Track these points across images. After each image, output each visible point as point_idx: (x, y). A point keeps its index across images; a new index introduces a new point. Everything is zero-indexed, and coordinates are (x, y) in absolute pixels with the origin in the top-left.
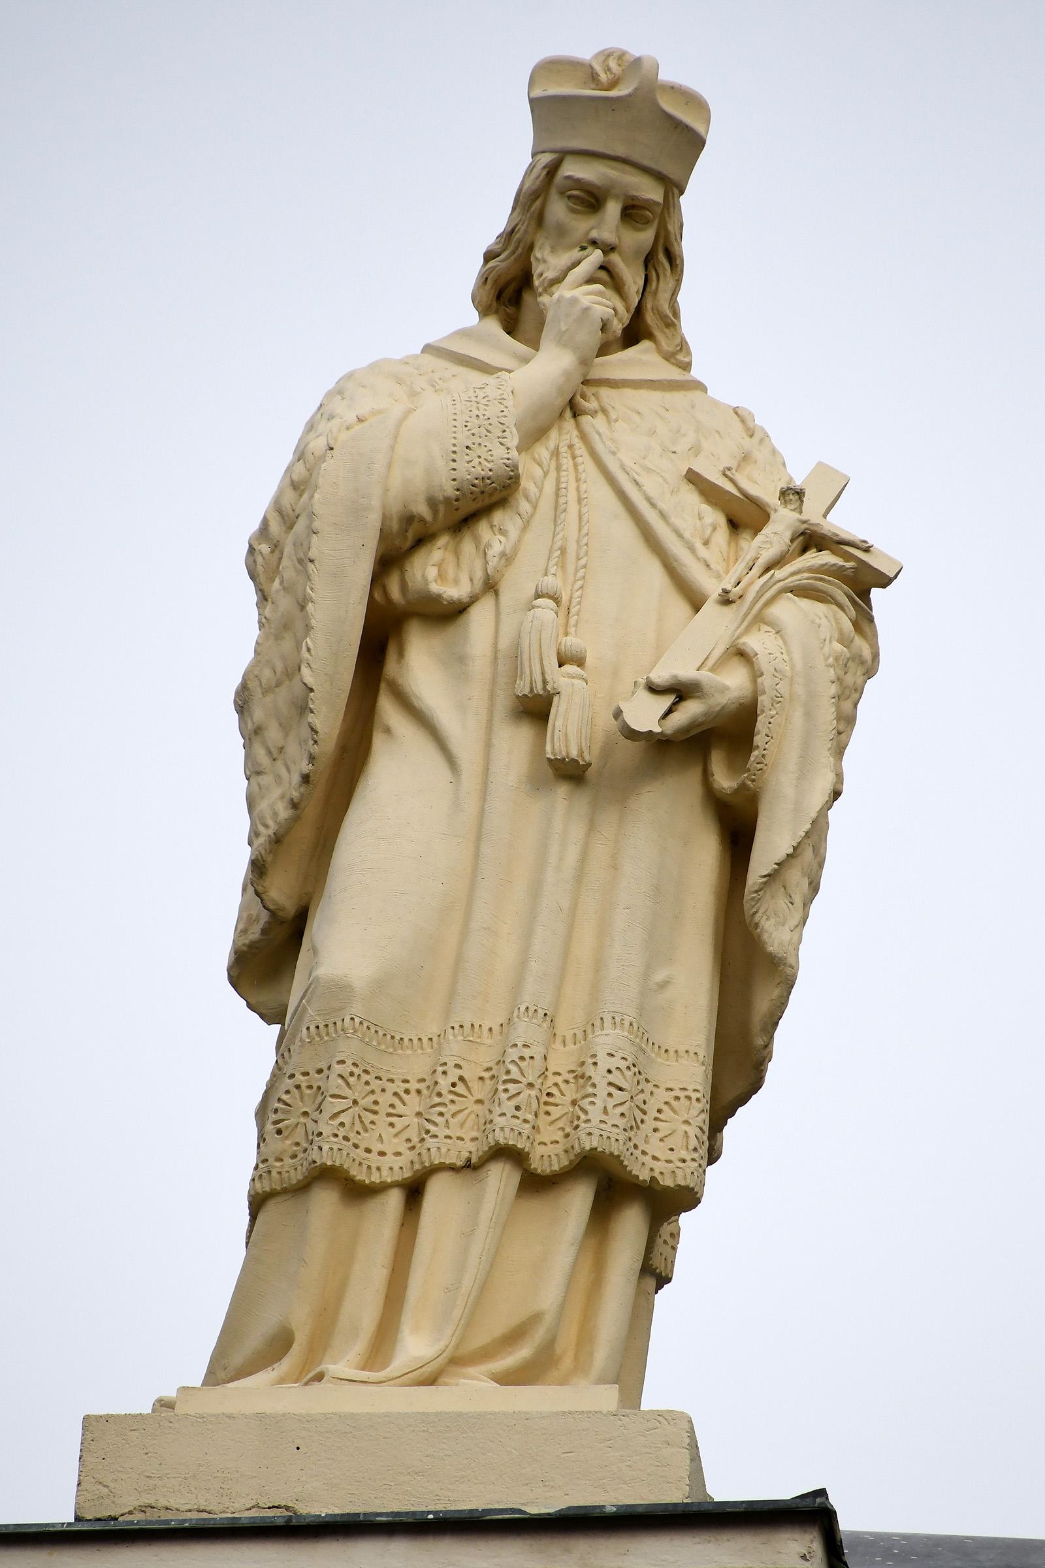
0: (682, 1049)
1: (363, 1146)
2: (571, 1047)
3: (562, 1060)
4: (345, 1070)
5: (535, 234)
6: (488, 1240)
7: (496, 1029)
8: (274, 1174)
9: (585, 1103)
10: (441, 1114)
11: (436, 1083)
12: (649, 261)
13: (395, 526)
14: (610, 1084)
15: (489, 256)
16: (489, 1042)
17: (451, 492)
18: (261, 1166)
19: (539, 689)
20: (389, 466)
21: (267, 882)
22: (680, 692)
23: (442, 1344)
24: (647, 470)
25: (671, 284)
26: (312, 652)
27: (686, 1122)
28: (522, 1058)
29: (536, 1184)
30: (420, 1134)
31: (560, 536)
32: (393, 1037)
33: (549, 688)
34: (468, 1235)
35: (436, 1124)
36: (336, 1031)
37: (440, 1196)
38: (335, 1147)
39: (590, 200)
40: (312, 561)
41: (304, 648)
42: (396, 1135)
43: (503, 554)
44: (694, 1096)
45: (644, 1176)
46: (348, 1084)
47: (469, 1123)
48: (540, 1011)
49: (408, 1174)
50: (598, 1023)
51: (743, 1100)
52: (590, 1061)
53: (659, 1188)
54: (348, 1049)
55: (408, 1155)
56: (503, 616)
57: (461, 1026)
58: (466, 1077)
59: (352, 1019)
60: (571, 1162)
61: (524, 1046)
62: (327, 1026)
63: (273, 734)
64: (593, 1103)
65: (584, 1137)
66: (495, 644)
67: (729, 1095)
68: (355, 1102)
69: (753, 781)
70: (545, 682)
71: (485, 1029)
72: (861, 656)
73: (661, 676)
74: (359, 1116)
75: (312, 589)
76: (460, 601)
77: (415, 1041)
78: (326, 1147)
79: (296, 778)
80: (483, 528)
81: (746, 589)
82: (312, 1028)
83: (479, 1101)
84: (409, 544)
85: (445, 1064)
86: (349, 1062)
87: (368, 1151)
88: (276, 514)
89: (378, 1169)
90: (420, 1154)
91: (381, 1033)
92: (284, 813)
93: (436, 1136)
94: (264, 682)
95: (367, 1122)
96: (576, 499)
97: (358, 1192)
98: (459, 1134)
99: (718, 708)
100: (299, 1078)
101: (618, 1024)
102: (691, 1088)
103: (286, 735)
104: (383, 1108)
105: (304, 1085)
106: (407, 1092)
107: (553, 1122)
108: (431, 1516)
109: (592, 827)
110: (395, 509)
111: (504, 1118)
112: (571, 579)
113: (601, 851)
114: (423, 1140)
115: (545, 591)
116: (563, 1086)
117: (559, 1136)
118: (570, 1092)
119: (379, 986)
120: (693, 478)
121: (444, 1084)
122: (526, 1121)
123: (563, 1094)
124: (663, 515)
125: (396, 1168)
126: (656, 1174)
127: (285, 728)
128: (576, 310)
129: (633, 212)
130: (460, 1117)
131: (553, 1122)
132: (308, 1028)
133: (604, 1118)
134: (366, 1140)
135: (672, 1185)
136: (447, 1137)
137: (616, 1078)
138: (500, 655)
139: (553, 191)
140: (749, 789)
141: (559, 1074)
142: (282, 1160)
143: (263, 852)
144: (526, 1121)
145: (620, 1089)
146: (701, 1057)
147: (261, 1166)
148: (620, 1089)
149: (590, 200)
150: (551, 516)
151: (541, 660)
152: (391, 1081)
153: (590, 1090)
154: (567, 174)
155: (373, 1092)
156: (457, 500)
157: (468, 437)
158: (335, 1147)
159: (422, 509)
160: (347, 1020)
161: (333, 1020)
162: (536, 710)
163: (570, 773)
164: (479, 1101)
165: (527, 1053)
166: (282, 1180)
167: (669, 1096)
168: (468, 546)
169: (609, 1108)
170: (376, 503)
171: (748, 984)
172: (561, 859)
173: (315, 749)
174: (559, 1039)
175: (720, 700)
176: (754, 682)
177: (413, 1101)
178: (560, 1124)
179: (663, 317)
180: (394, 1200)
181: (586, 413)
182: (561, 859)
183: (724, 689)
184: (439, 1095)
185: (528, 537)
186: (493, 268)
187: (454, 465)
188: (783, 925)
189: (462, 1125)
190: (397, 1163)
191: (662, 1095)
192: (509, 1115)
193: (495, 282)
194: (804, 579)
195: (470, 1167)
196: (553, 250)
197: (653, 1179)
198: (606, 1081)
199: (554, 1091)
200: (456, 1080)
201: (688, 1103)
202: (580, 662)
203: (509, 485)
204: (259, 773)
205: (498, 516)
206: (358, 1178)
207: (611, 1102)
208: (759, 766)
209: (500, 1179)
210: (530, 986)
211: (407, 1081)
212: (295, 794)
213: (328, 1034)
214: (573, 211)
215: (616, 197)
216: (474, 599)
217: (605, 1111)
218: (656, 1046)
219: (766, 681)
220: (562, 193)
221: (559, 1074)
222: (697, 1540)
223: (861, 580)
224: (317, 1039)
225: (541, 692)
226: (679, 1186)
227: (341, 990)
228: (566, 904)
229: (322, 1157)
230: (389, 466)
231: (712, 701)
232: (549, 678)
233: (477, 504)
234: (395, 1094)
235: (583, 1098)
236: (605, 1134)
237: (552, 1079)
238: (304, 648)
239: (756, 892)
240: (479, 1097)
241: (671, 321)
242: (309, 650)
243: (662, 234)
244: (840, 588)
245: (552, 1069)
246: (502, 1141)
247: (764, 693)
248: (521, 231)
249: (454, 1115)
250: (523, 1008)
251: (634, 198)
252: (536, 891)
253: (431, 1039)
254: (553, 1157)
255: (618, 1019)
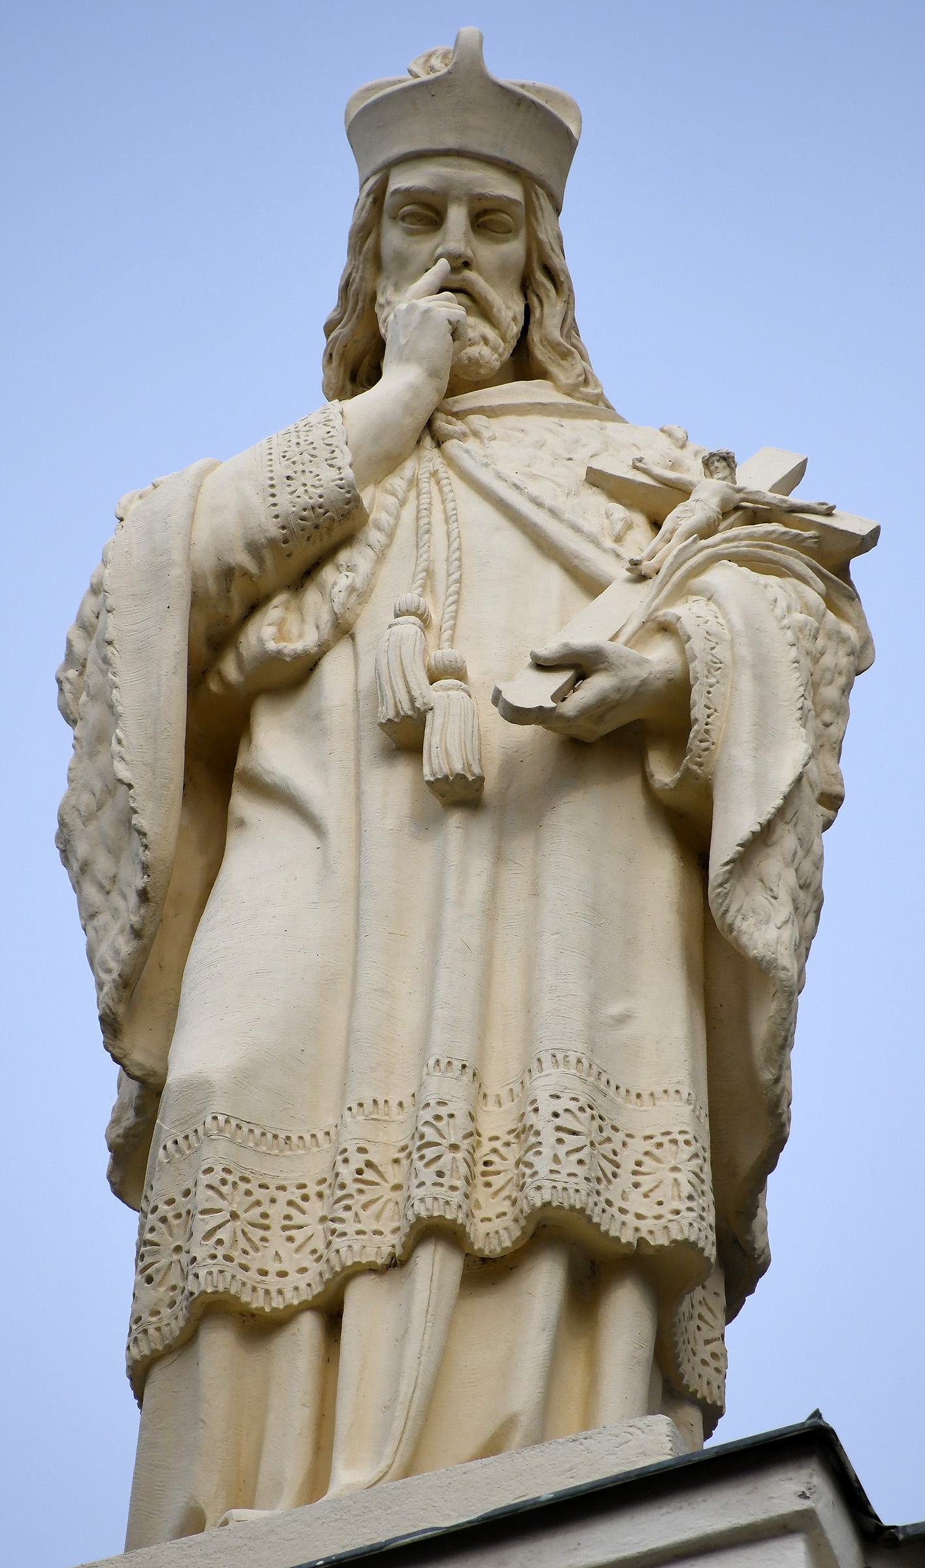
0: (658, 1090)
1: (254, 1266)
2: (507, 1105)
3: (496, 1122)
4: (214, 1179)
5: (375, 280)
6: (427, 1338)
7: (408, 1101)
8: (151, 1331)
9: (530, 1157)
10: (348, 1208)
11: (337, 1175)
12: (526, 286)
13: (212, 586)
14: (558, 1129)
15: (329, 329)
16: (401, 1117)
17: (274, 531)
18: (134, 1327)
19: (406, 708)
20: (192, 516)
21: (126, 1043)
22: (579, 665)
23: (383, 1465)
24: (534, 477)
25: (560, 307)
26: (124, 742)
27: (675, 1169)
28: (438, 1118)
29: (487, 1273)
30: (326, 1237)
31: (425, 556)
32: (275, 1137)
33: (418, 705)
34: (401, 1340)
35: (342, 1220)
36: (198, 1139)
37: (363, 1305)
38: (215, 1270)
39: (428, 213)
40: (110, 643)
41: (114, 741)
42: (298, 1250)
43: (352, 589)
44: (681, 1138)
45: (627, 1236)
46: (221, 1195)
47: (387, 1213)
48: (454, 1062)
49: (318, 1289)
50: (535, 1065)
51: (769, 1163)
52: (530, 1108)
53: (651, 1252)
54: (216, 1153)
55: (315, 1268)
56: (362, 657)
57: (361, 1105)
58: (375, 1161)
59: (215, 1118)
60: (523, 1229)
61: (439, 1103)
62: (186, 1137)
63: (103, 865)
64: (539, 1153)
65: (532, 1193)
66: (356, 685)
67: (748, 1160)
68: (234, 1216)
69: (700, 765)
70: (412, 700)
71: (393, 1104)
72: (839, 632)
73: (549, 647)
74: (243, 1232)
75: (114, 674)
76: (306, 654)
77: (307, 1138)
78: (202, 1273)
79: (133, 899)
80: (328, 574)
81: (662, 561)
82: (170, 1145)
83: (397, 1187)
84: (237, 611)
85: (345, 1150)
86: (218, 1168)
87: (264, 1273)
88: (80, 632)
89: (280, 1292)
90: (328, 1261)
91: (257, 1132)
92: (126, 946)
93: (344, 1234)
94: (82, 809)
95: (256, 1239)
96: (442, 516)
97: (260, 1328)
98: (375, 1227)
99: (636, 682)
100: (163, 1208)
101: (561, 1062)
102: (675, 1130)
103: (117, 860)
104: (276, 1221)
105: (170, 1215)
106: (305, 1198)
107: (496, 1193)
108: (321, 1562)
109: (499, 857)
110: (207, 563)
111: (422, 1189)
112: (442, 597)
113: (515, 882)
114: (329, 1244)
115: (404, 609)
116: (503, 1150)
117: (506, 1206)
118: (513, 1154)
119: (246, 1076)
120: (596, 479)
121: (347, 1173)
122: (453, 1188)
123: (504, 1159)
124: (553, 513)
125: (302, 1286)
126: (644, 1234)
127: (115, 853)
128: (416, 317)
129: (486, 219)
130: (375, 1208)
131: (496, 1193)
132: (165, 1148)
133: (555, 1167)
134: (256, 1261)
135: (666, 1243)
136: (359, 1233)
137: (565, 1121)
138: (360, 697)
139: (386, 222)
140: (697, 777)
141: (497, 1138)
142: (159, 1313)
143: (111, 1003)
144: (453, 1188)
145: (574, 1133)
146: (685, 1095)
147: (134, 1327)
148: (574, 1133)
149: (428, 213)
150: (413, 540)
151: (405, 676)
152: (282, 1188)
153: (533, 1139)
154: (396, 187)
155: (258, 1203)
156: (285, 542)
157: (288, 467)
158: (215, 1270)
159: (242, 558)
160: (209, 1120)
161: (193, 1128)
162: (405, 738)
163: (460, 795)
164: (397, 1187)
165: (443, 1111)
166: (163, 1339)
167: (649, 1146)
168: (312, 596)
169: (562, 1156)
170: (177, 556)
171: (738, 1009)
172: (461, 893)
173: (147, 856)
174: (491, 1100)
175: (635, 674)
176: (682, 651)
177: (316, 1208)
178: (505, 1193)
179: (555, 347)
180: (308, 1327)
181: (452, 437)
182: (461, 893)
183: (641, 662)
184: (343, 1186)
185: (386, 571)
186: (338, 337)
187: (273, 500)
188: (767, 922)
189: (378, 1217)
190: (302, 1281)
191: (638, 1146)
192: (429, 1183)
193: (343, 356)
194: (742, 547)
195: (397, 1264)
196: (397, 287)
197: (641, 1241)
198: (551, 1126)
199: (493, 1157)
200: (363, 1166)
201: (674, 1148)
202: (459, 673)
203: (349, 512)
204: (92, 916)
205: (343, 557)
206: (254, 1306)
207: (562, 1150)
208: (704, 745)
209: (435, 1267)
210: (439, 1036)
211: (303, 1186)
212: (135, 919)
213: (190, 1147)
214: (410, 233)
215: (458, 199)
216: (324, 649)
217: (556, 1159)
218: (622, 1091)
219: (696, 645)
220: (394, 218)
221: (497, 1138)
222: (665, 1510)
223: (834, 557)
224: (177, 1156)
225: (410, 713)
226: (675, 1241)
227: (199, 1087)
228: (475, 940)
229: (199, 1284)
230: (192, 516)
231: (624, 674)
232: (416, 694)
233: (314, 542)
234: (291, 1203)
235: (527, 1152)
236: (560, 1186)
237: (487, 1146)
238: (114, 741)
239: (721, 885)
240: (396, 1181)
241: (569, 347)
242: (119, 742)
243: (534, 246)
244: (798, 557)
245: (487, 1133)
246: (424, 1214)
247: (695, 658)
248: (357, 280)
249: (365, 1207)
250: (432, 1062)
251: (481, 197)
252: (435, 936)
253: (327, 1133)
254: (502, 1232)
255: (560, 1056)
